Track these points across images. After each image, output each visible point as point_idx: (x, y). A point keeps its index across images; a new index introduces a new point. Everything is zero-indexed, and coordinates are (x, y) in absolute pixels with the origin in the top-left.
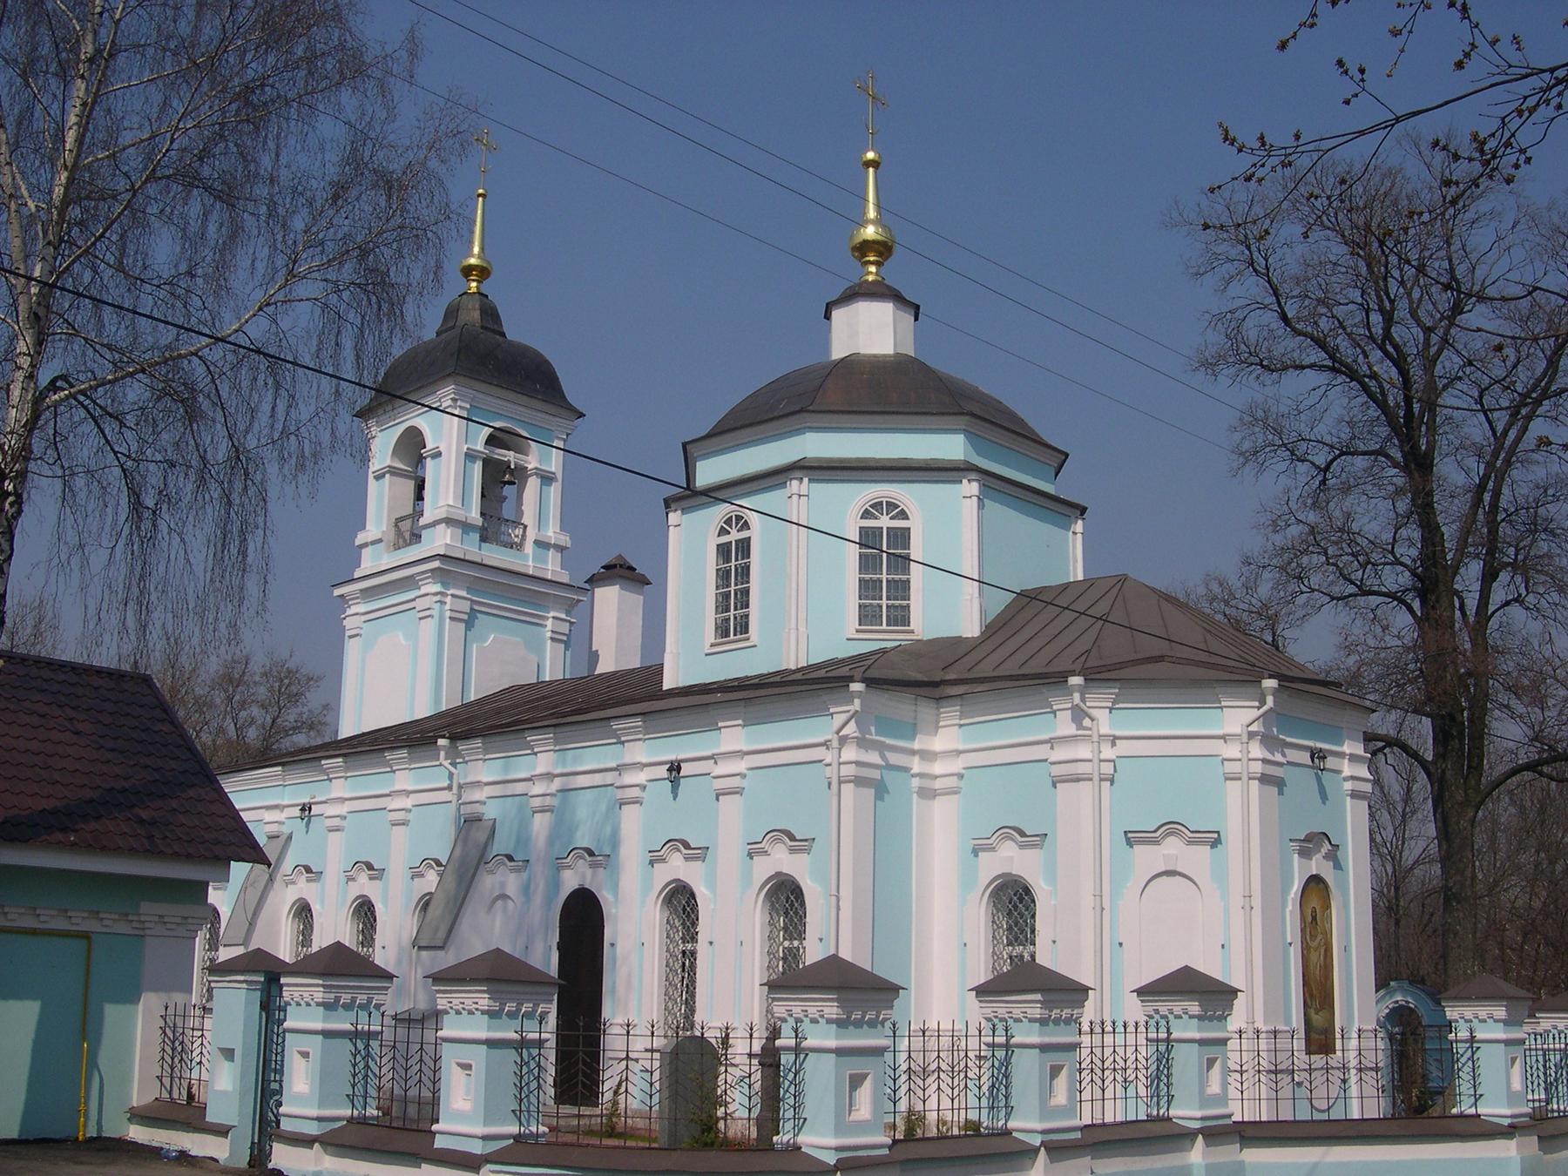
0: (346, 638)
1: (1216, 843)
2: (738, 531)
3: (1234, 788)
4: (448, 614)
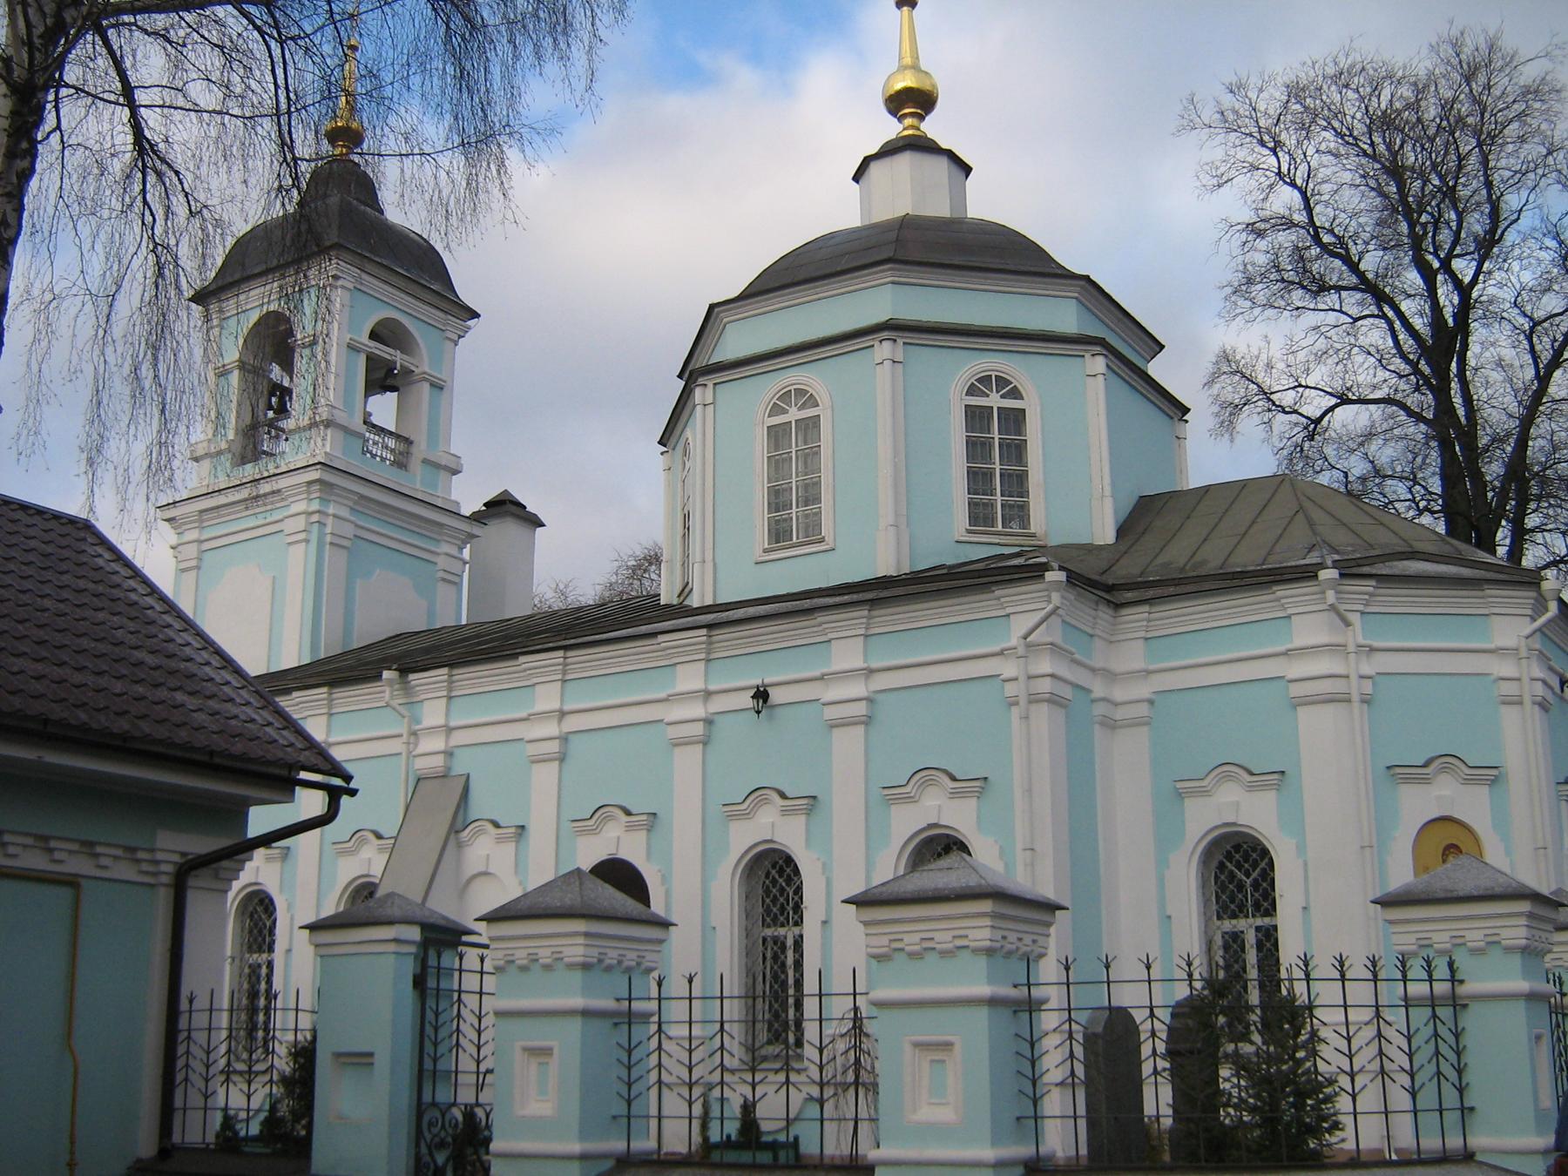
1: (1494, 782)
2: (799, 409)
3: (1510, 716)
4: (328, 539)
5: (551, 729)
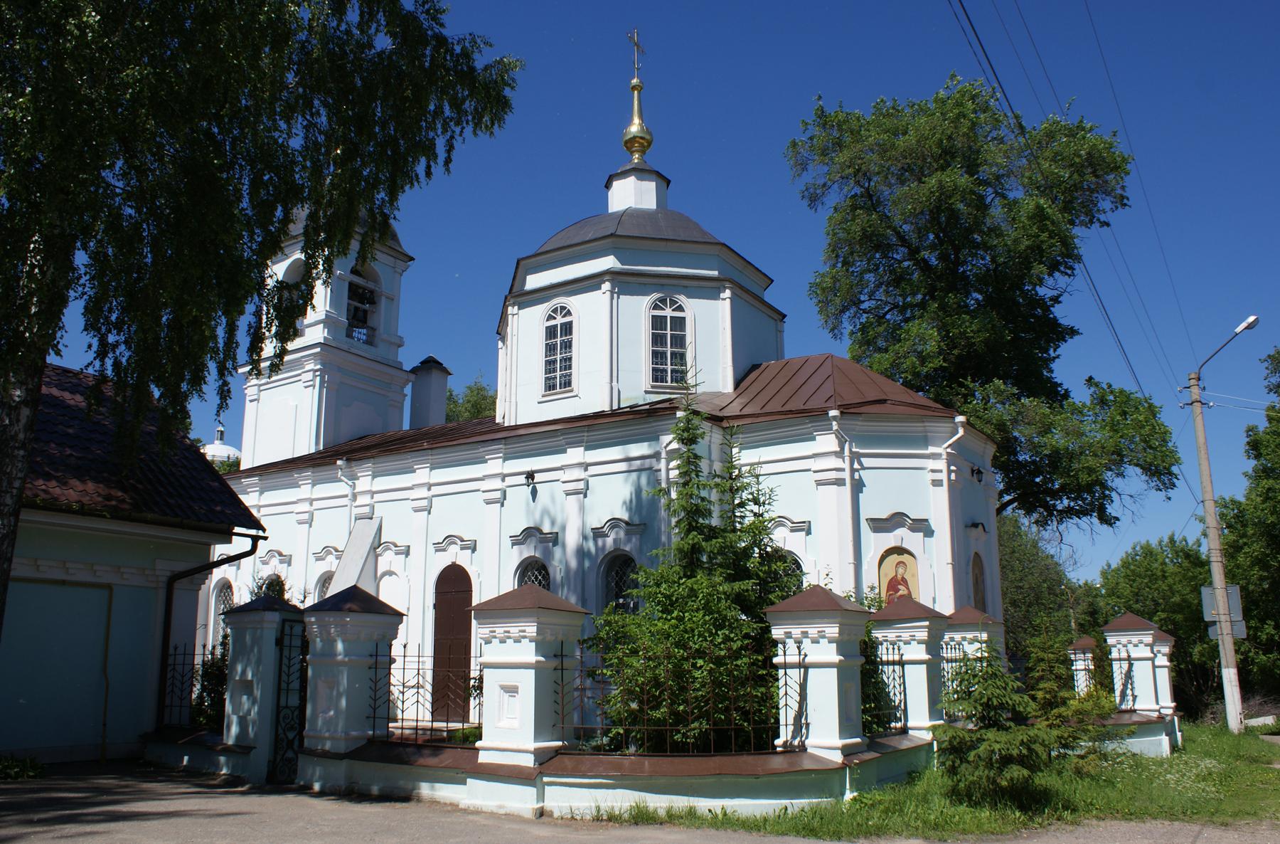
0: (247, 402)
5: (423, 492)
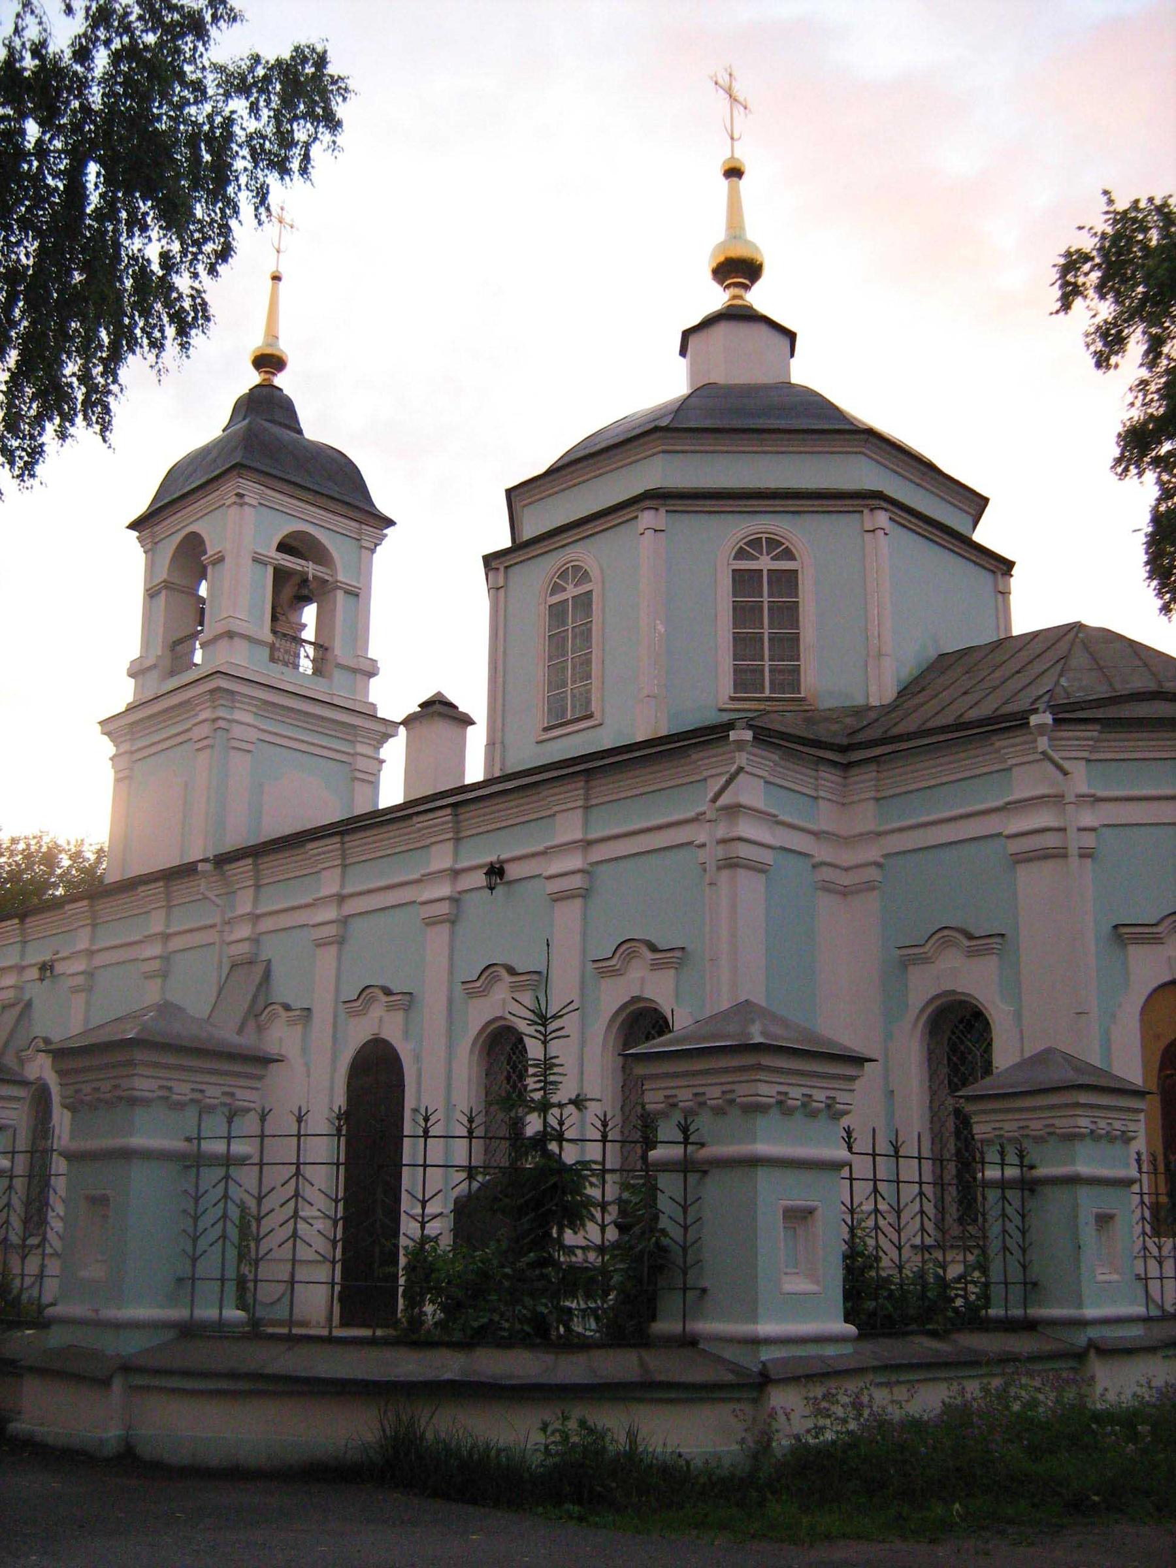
2: (576, 586)
